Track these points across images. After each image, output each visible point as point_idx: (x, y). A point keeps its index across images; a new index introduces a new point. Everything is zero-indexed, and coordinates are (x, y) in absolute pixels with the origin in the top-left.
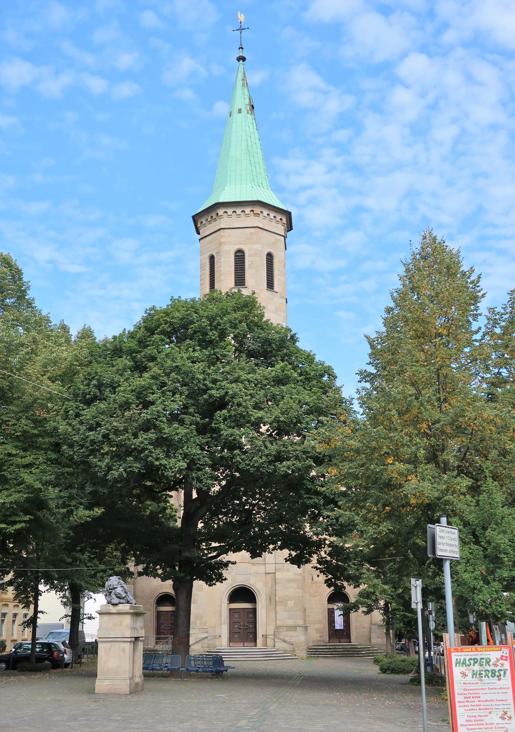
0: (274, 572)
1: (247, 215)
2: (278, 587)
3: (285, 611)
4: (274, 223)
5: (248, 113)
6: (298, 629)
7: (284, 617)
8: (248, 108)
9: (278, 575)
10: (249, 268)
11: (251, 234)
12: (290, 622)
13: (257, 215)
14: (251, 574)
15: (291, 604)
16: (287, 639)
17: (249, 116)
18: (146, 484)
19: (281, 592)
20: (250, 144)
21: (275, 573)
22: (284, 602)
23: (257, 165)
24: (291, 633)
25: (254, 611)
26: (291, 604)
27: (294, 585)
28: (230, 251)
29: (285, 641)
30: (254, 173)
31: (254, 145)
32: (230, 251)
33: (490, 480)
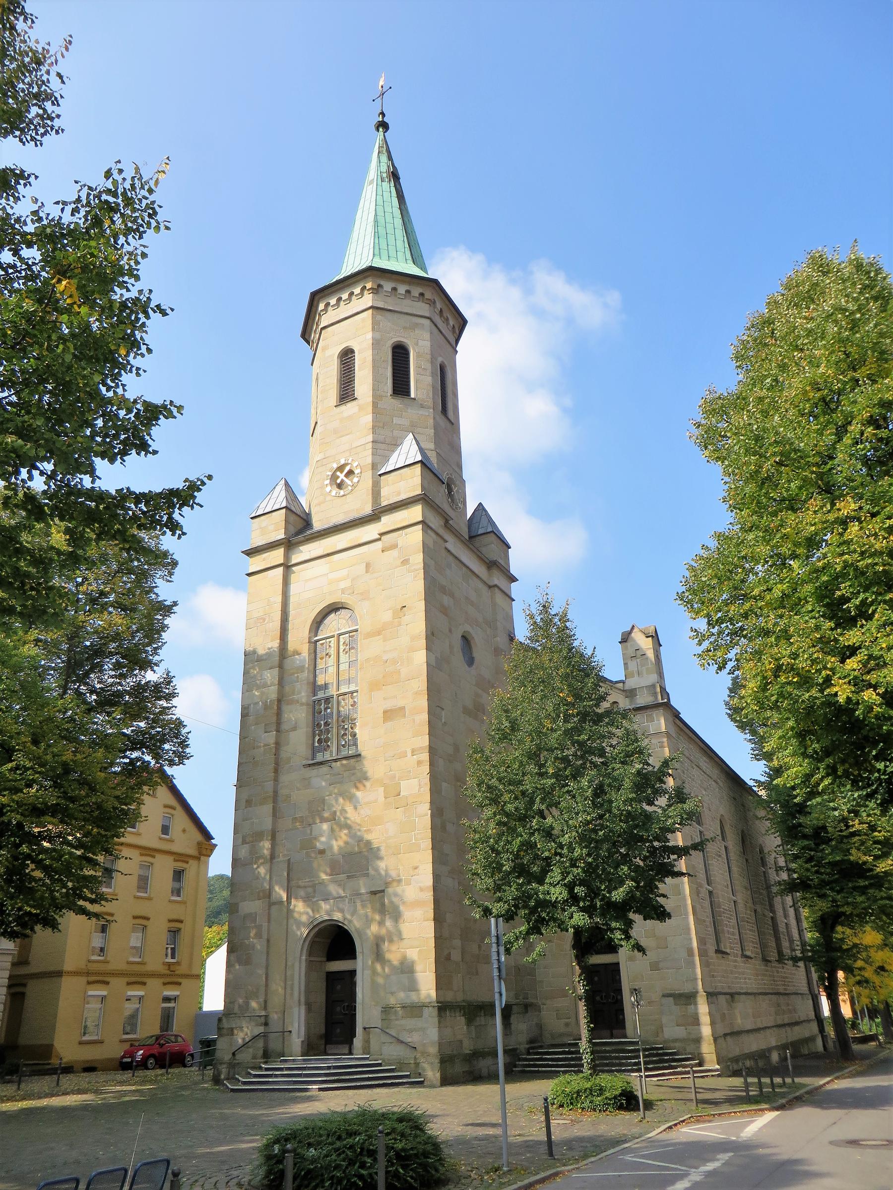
4: (408, 302)
8: (385, 175)
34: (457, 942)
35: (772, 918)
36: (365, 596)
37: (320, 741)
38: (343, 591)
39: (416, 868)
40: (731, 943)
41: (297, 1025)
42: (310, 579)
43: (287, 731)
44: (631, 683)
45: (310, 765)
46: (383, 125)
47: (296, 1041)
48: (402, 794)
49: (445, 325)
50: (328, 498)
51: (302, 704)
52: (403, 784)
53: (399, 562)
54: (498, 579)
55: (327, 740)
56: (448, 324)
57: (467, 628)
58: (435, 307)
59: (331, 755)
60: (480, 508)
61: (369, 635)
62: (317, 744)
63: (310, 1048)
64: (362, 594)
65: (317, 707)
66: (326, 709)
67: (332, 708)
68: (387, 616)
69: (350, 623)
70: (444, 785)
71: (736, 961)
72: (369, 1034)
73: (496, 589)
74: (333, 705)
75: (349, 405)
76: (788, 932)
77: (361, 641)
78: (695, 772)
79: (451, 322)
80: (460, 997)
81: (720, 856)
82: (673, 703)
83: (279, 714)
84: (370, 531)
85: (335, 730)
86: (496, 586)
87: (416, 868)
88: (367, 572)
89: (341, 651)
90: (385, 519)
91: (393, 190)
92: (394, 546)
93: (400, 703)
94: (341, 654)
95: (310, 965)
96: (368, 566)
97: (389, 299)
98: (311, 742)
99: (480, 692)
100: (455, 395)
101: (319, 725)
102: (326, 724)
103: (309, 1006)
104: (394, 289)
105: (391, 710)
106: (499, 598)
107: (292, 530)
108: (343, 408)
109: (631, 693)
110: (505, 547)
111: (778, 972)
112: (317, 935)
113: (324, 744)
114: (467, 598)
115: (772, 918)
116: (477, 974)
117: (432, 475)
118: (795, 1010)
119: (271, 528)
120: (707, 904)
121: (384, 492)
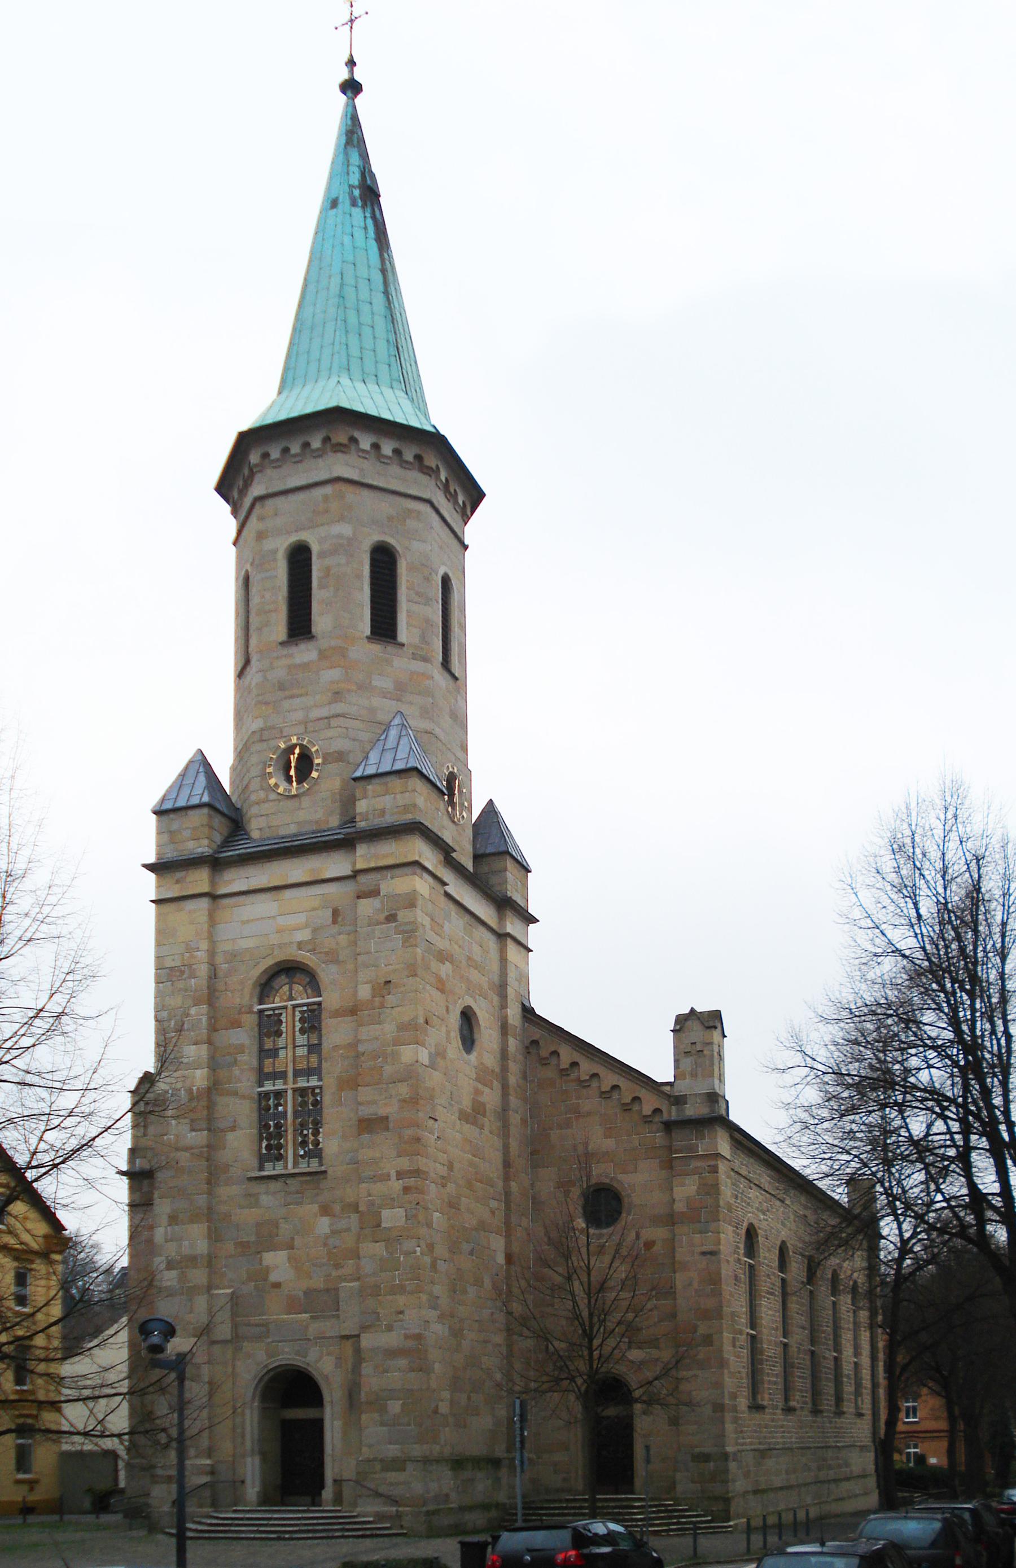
0: (357, 1333)
1: (319, 454)
2: (367, 1369)
3: (382, 1424)
4: (395, 469)
5: (354, 204)
6: (410, 1466)
7: (376, 1437)
8: (357, 193)
9: (367, 1341)
10: (321, 587)
11: (326, 498)
12: (393, 1450)
13: (340, 448)
14: (309, 1340)
15: (395, 1407)
16: (382, 1489)
17: (357, 212)
18: (969, 1522)
19: (372, 1381)
20: (350, 280)
21: (358, 1336)
22: (378, 1403)
23: (367, 331)
24: (392, 1476)
25: (318, 1426)
26: (395, 1407)
27: (403, 1362)
28: (275, 551)
29: (378, 1494)
30: (355, 352)
31: (363, 285)
32: (275, 551)
33: (447, 717)
34: (446, 1395)
35: (836, 1359)
36: (332, 957)
37: (269, 1147)
38: (300, 945)
39: (401, 1312)
40: (770, 1394)
41: (252, 1475)
42: (248, 921)
43: (222, 1131)
44: (683, 1088)
45: (256, 1178)
46: (351, 87)
47: (252, 1491)
48: (383, 1225)
49: (450, 505)
50: (273, 796)
51: (243, 1097)
52: (385, 1213)
53: (382, 917)
54: (512, 926)
55: (280, 1147)
56: (456, 502)
57: (469, 1001)
58: (438, 477)
59: (286, 1167)
60: (490, 810)
61: (337, 1014)
62: (264, 1151)
63: (265, 1499)
64: (326, 953)
65: (263, 1103)
66: (277, 1106)
67: (285, 1106)
68: (364, 992)
69: (309, 991)
70: (437, 1215)
71: (774, 1414)
72: (341, 1486)
73: (509, 941)
74: (286, 1102)
75: (303, 646)
76: (856, 1375)
77: (328, 1023)
78: (753, 1193)
79: (461, 500)
80: (447, 1451)
81: (772, 1294)
82: (734, 1117)
83: (211, 1107)
84: (336, 865)
85: (290, 1137)
86: (509, 935)
87: (401, 1312)
88: (335, 922)
89: (297, 1029)
90: (361, 850)
91: (370, 222)
92: (375, 893)
93: (382, 1112)
94: (297, 1033)
95: (264, 1411)
96: (336, 913)
97: (366, 464)
98: (256, 1148)
99: (480, 1086)
100: (463, 627)
101: (267, 1126)
102: (278, 1126)
103: (263, 1455)
104: (376, 446)
105: (369, 1120)
106: (511, 948)
107: (218, 839)
108: (293, 650)
109: (679, 1101)
110: (523, 872)
111: (830, 1422)
112: (272, 1380)
113: (274, 1153)
114: (469, 958)
115: (836, 1359)
116: (465, 1426)
117: (429, 786)
118: (847, 1465)
119: (187, 834)
120: (745, 1353)
121: (362, 806)
